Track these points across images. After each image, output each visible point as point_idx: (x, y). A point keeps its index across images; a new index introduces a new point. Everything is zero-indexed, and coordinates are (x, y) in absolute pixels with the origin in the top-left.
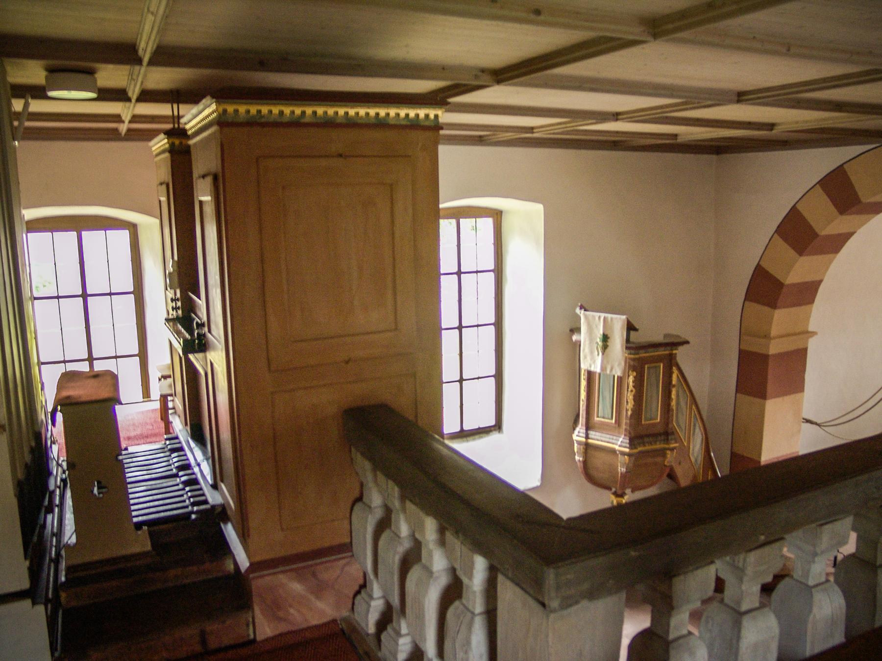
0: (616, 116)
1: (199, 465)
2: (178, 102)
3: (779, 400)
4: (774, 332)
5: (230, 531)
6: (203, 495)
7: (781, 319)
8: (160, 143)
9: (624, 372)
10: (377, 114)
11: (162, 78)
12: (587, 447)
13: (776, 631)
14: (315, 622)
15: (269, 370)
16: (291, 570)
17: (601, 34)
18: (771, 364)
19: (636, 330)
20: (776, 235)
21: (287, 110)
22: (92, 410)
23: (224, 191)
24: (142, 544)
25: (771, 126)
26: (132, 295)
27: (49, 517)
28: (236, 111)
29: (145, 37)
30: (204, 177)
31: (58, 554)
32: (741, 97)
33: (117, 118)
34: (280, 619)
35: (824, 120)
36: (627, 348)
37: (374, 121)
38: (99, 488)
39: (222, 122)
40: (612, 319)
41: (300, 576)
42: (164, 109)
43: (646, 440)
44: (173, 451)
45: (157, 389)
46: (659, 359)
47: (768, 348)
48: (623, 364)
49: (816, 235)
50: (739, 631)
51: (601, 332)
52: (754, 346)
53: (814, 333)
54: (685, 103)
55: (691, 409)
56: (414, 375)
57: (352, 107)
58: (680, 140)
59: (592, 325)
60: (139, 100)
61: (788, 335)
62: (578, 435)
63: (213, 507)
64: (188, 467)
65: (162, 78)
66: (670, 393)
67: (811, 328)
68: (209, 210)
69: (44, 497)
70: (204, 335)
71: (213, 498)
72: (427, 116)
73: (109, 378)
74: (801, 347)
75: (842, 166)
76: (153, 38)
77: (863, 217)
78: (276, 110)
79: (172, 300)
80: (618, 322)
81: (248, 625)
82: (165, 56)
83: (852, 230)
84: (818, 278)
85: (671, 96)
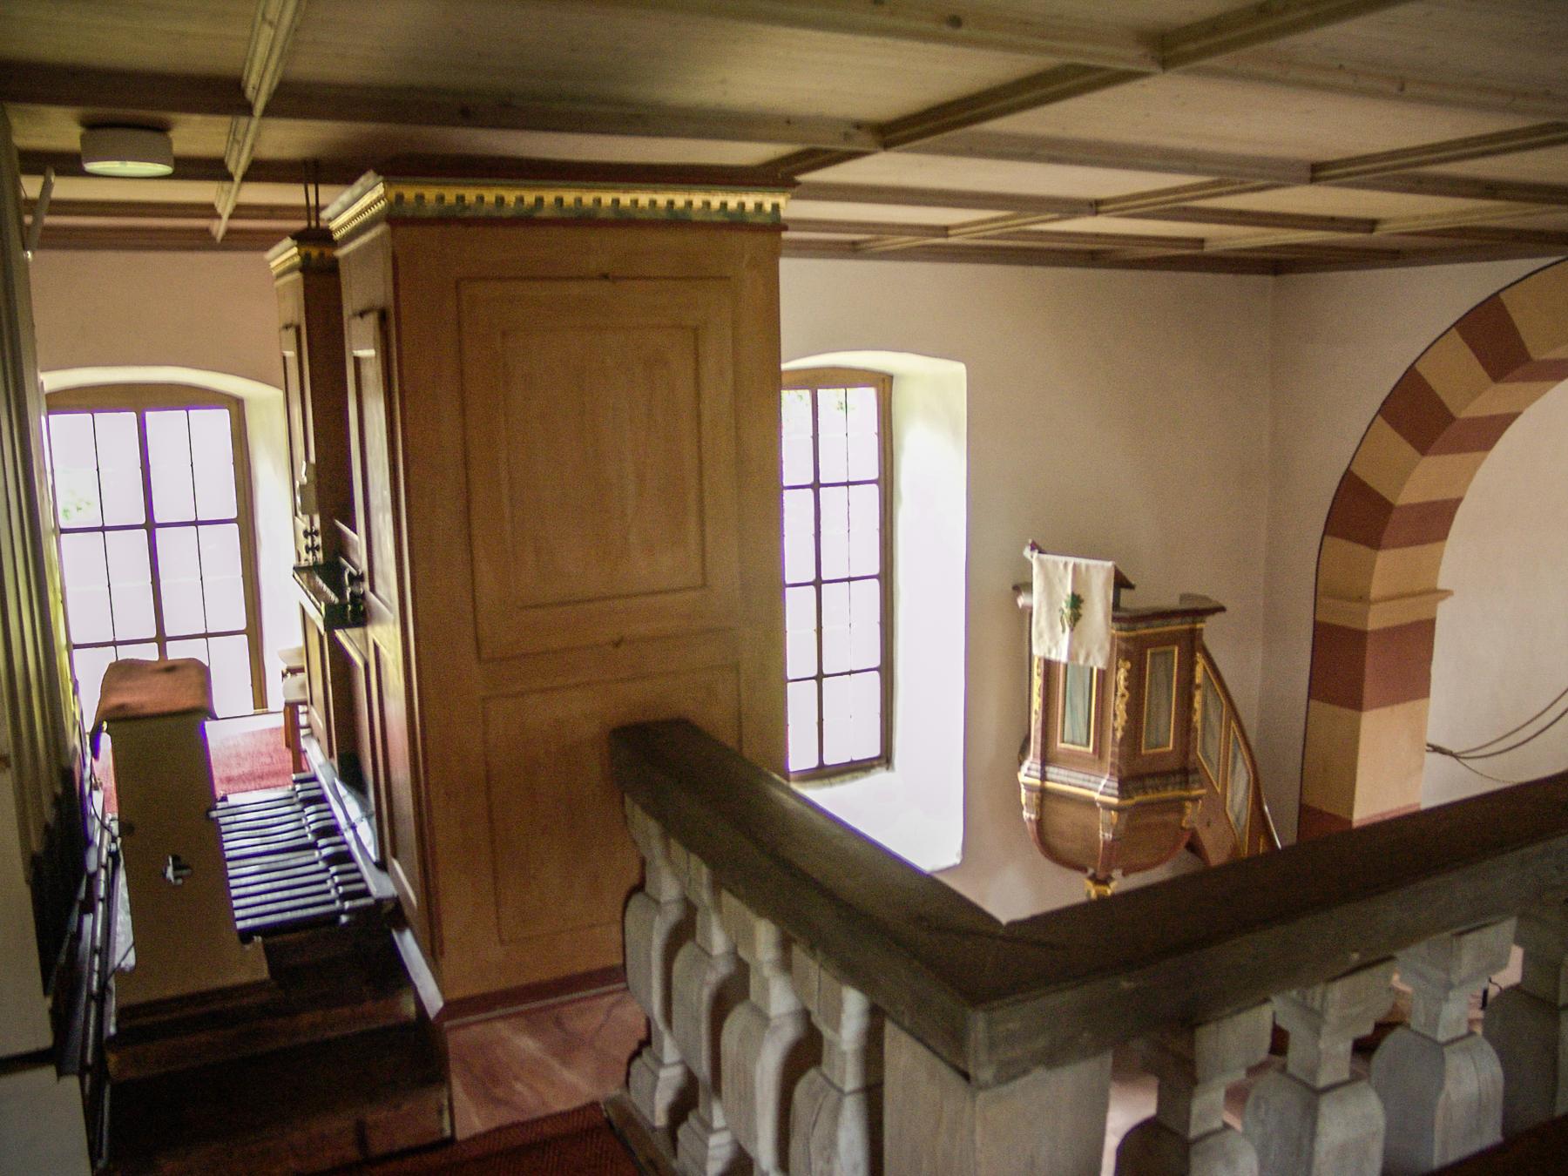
0: (1095, 207)
1: (353, 827)
2: (317, 182)
3: (1385, 712)
4: (1375, 591)
5: (409, 945)
6: (362, 880)
7: (1389, 567)
8: (285, 254)
9: (1109, 662)
10: (671, 203)
11: (287, 138)
12: (1044, 796)
13: (1380, 1122)
14: (560, 1106)
15: (479, 658)
16: (518, 1014)
17: (1069, 60)
18: (1371, 647)
19: (1130, 586)
20: (1379, 418)
21: (510, 196)
22: (163, 730)
23: (399, 340)
24: (252, 967)
25: (1371, 225)
26: (235, 526)
27: (88, 920)
28: (420, 198)
29: (257, 67)
30: (362, 314)
31: (103, 986)
32: (1317, 172)
33: (209, 210)
34: (497, 1102)
35: (1466, 213)
36: (1115, 619)
37: (664, 215)
38: (175, 868)
39: (395, 217)
40: (1088, 567)
41: (533, 1024)
42: (291, 195)
43: (1149, 782)
44: (308, 802)
45: (279, 691)
46: (1172, 639)
47: (1366, 619)
48: (1107, 647)
49: (1451, 418)
50: (1314, 1123)
51: (1069, 591)
52: (1341, 616)
53: (1447, 593)
54: (1219, 184)
55: (1228, 727)
56: (736, 668)
57: (626, 191)
58: (1208, 249)
59: (1052, 579)
60: (247, 178)
61: (1402, 596)
62: (1028, 774)
63: (379, 902)
64: (334, 830)
65: (287, 138)
66: (1191, 698)
67: (1442, 584)
68: (372, 374)
69: (78, 885)
70: (363, 596)
71: (379, 886)
72: (759, 206)
73: (193, 672)
74: (1424, 617)
75: (1496, 294)
76: (272, 67)
77: (1535, 386)
78: (490, 196)
79: (306, 534)
80: (1099, 573)
81: (440, 1112)
82: (293, 99)
83: (1514, 410)
84: (1453, 495)
85: (1193, 171)
